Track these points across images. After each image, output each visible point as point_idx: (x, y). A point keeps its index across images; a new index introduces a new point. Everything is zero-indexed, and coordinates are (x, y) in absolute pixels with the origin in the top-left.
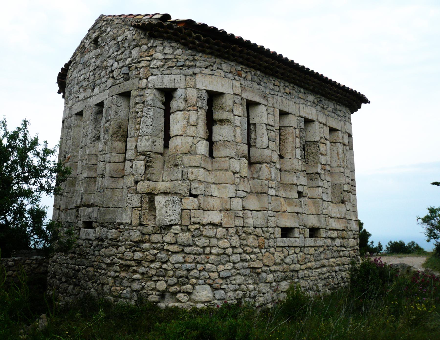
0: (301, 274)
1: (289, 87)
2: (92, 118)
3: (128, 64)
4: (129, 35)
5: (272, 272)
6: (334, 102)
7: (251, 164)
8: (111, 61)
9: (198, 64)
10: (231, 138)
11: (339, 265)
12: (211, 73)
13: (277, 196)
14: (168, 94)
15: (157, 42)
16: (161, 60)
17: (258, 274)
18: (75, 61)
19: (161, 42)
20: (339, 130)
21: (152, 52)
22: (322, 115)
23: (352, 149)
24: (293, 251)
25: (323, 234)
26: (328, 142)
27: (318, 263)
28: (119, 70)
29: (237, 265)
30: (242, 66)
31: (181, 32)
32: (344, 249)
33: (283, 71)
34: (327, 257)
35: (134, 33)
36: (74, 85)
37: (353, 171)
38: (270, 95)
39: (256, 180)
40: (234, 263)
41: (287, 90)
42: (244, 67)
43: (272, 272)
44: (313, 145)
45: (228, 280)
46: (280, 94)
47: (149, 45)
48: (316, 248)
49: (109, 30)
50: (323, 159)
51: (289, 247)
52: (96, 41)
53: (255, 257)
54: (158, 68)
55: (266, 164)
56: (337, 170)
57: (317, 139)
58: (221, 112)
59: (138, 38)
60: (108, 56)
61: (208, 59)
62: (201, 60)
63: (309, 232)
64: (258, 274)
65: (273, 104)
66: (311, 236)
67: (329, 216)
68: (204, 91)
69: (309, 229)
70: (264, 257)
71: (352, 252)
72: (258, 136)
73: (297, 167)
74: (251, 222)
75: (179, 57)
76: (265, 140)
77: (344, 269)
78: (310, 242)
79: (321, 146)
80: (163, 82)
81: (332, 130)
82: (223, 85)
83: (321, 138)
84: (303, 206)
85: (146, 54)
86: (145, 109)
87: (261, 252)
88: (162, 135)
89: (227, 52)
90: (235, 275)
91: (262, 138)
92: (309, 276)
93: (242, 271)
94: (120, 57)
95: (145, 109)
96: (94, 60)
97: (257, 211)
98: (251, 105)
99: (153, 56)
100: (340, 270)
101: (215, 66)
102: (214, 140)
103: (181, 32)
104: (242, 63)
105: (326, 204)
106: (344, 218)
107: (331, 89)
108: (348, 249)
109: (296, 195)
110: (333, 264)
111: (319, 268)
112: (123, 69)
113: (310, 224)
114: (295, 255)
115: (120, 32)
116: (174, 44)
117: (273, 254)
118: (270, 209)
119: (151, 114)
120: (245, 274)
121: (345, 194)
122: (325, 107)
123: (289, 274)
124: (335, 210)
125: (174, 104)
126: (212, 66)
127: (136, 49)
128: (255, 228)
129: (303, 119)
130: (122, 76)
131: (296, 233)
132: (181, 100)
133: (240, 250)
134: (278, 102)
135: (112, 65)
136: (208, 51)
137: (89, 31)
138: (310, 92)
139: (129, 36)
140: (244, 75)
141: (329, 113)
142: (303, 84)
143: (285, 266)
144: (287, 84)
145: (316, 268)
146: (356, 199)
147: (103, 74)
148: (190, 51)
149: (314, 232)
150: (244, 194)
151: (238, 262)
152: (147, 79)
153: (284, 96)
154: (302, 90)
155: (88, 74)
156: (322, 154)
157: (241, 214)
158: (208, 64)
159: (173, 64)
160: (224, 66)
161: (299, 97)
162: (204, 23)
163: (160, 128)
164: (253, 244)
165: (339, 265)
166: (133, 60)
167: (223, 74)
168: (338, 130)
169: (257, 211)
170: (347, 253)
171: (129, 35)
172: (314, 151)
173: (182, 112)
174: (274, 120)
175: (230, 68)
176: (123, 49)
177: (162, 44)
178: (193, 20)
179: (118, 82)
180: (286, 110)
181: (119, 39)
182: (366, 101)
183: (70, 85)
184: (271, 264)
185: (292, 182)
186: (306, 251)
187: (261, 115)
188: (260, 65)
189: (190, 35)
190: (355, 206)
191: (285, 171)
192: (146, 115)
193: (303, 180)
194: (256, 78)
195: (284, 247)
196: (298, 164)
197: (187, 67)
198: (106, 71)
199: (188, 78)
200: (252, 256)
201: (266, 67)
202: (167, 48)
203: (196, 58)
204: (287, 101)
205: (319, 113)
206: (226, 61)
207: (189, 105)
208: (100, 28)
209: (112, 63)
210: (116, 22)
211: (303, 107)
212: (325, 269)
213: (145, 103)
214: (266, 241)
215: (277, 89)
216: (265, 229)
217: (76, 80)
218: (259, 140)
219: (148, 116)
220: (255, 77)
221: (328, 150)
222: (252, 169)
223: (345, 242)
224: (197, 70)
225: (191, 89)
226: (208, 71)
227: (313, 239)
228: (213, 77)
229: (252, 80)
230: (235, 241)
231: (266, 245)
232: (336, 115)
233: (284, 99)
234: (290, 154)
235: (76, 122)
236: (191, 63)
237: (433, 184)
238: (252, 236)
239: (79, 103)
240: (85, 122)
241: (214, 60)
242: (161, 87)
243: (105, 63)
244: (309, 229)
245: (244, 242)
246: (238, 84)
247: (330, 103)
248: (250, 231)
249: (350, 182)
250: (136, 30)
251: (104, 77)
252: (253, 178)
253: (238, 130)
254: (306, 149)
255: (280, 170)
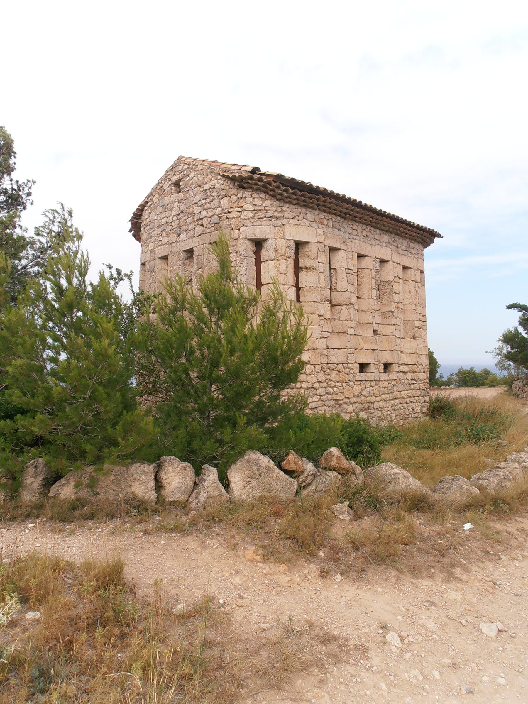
0: (376, 405)
1: (367, 230)
2: (180, 264)
3: (218, 214)
4: (217, 184)
5: (352, 403)
6: (408, 240)
7: (332, 306)
8: (197, 209)
9: (286, 215)
10: (316, 284)
11: (410, 397)
12: (298, 223)
13: (356, 335)
14: (259, 244)
15: (247, 194)
16: (252, 211)
17: (340, 405)
18: (152, 202)
19: (250, 193)
20: (411, 268)
21: (242, 203)
22: (396, 254)
23: (424, 285)
24: (370, 385)
25: (395, 368)
26: (401, 281)
27: (391, 395)
28: (209, 219)
29: (323, 398)
30: (324, 214)
31: (270, 184)
32: (414, 382)
33: (361, 216)
34: (399, 390)
35: (222, 182)
36: (153, 227)
37: (424, 307)
38: (349, 240)
39: (337, 321)
40: (321, 396)
41: (365, 233)
42: (326, 214)
43: (352, 403)
44: (387, 284)
45: (316, 410)
46: (358, 238)
47: (239, 196)
48: (390, 382)
49: (192, 175)
50: (396, 298)
51: (366, 380)
52: (177, 184)
53: (338, 390)
54: (248, 219)
55: (346, 306)
56: (410, 307)
57: (391, 278)
58: (306, 259)
59: (227, 188)
60: (193, 202)
61: (295, 210)
62: (288, 210)
63: (383, 367)
64: (340, 405)
65: (351, 249)
66: (385, 371)
67: (401, 352)
68: (292, 241)
69: (384, 364)
70: (345, 390)
71: (422, 385)
72: (338, 280)
73: (373, 308)
74: (334, 359)
75: (269, 208)
76: (345, 283)
77: (415, 401)
78: (384, 376)
79: (395, 284)
80: (254, 234)
81: (405, 268)
82: (308, 235)
83: (395, 277)
84: (378, 344)
85: (236, 205)
86: (239, 259)
87: (342, 386)
88: (254, 282)
89: (312, 203)
90: (321, 406)
91: (342, 281)
92: (383, 407)
93: (326, 403)
94: (209, 205)
95: (239, 259)
96: (177, 204)
97: (339, 349)
98: (332, 250)
99: (244, 207)
100: (411, 402)
101: (301, 216)
102: (300, 286)
103: (270, 184)
104: (324, 211)
105: (398, 341)
106: (415, 353)
107: (405, 229)
108: (418, 383)
109: (372, 333)
110: (404, 396)
111: (392, 400)
112: (213, 218)
113: (384, 361)
114: (371, 388)
115: (206, 180)
116: (263, 196)
117: (352, 387)
118: (349, 347)
119: (245, 263)
120: (329, 405)
121: (416, 331)
122: (399, 246)
123: (367, 405)
124: (409, 346)
125: (264, 254)
126: (299, 216)
127: (225, 198)
128: (337, 364)
129: (379, 260)
130: (213, 225)
131: (372, 368)
132: (272, 250)
133: (325, 385)
134: (356, 246)
135: (200, 212)
136: (295, 202)
137: (167, 172)
138: (385, 233)
139: (217, 186)
140: (326, 223)
141: (402, 251)
142: (379, 226)
143: (363, 398)
144: (364, 226)
145: (389, 400)
146: (426, 334)
147: (190, 220)
148: (278, 202)
149: (387, 367)
150: (328, 334)
151: (324, 395)
152: (239, 230)
153: (361, 239)
154: (378, 231)
155: (171, 218)
156: (395, 293)
157: (325, 352)
158: (295, 214)
159: (263, 216)
160: (309, 215)
161: (375, 239)
162: (293, 177)
163: (253, 276)
164: (336, 379)
165: (410, 397)
166: (223, 210)
167: (308, 223)
168: (411, 268)
169: (339, 349)
170: (418, 386)
171: (217, 184)
172: (388, 290)
173: (273, 262)
174: (353, 264)
175: (314, 217)
176: (211, 198)
177: (251, 195)
178: (283, 174)
179: (208, 231)
180: (363, 253)
181: (206, 187)
182: (439, 236)
183: (148, 227)
184: (351, 396)
185: (368, 322)
186: (381, 384)
187: (341, 260)
188: (341, 212)
189: (278, 187)
190: (425, 341)
191: (362, 311)
192: (240, 265)
193: (378, 319)
194: (336, 225)
195: (362, 381)
196: (373, 304)
197: (276, 218)
198: (193, 218)
199: (277, 228)
200: (335, 389)
201: (346, 214)
202: (256, 199)
203: (284, 209)
204: (364, 243)
205: (393, 252)
206: (311, 210)
207: (280, 255)
208: (182, 171)
209: (199, 211)
210: (200, 167)
211: (378, 247)
212: (397, 401)
213: (238, 253)
214: (346, 375)
215: (355, 233)
216: (345, 365)
217: (156, 223)
218: (339, 284)
219: (242, 265)
220: (336, 223)
221: (401, 288)
222: (333, 310)
223: (415, 376)
224: (285, 221)
225: (280, 239)
226: (294, 221)
227: (387, 373)
228: (300, 226)
229: (333, 227)
230: (321, 376)
231: (347, 379)
232: (409, 253)
233: (361, 242)
234: (367, 294)
235: (160, 266)
236: (280, 215)
237: (509, 307)
238: (335, 372)
239: (162, 247)
240: (172, 266)
241: (300, 210)
242: (253, 238)
243: (191, 210)
244: (384, 364)
245: (328, 377)
246: (321, 232)
247: (403, 241)
248: (333, 367)
249: (421, 317)
250: (224, 179)
251: (191, 223)
252: (334, 319)
253: (322, 276)
254: (380, 289)
255: (358, 311)
